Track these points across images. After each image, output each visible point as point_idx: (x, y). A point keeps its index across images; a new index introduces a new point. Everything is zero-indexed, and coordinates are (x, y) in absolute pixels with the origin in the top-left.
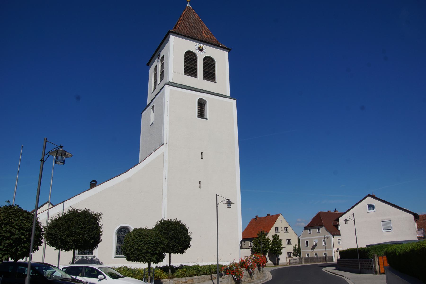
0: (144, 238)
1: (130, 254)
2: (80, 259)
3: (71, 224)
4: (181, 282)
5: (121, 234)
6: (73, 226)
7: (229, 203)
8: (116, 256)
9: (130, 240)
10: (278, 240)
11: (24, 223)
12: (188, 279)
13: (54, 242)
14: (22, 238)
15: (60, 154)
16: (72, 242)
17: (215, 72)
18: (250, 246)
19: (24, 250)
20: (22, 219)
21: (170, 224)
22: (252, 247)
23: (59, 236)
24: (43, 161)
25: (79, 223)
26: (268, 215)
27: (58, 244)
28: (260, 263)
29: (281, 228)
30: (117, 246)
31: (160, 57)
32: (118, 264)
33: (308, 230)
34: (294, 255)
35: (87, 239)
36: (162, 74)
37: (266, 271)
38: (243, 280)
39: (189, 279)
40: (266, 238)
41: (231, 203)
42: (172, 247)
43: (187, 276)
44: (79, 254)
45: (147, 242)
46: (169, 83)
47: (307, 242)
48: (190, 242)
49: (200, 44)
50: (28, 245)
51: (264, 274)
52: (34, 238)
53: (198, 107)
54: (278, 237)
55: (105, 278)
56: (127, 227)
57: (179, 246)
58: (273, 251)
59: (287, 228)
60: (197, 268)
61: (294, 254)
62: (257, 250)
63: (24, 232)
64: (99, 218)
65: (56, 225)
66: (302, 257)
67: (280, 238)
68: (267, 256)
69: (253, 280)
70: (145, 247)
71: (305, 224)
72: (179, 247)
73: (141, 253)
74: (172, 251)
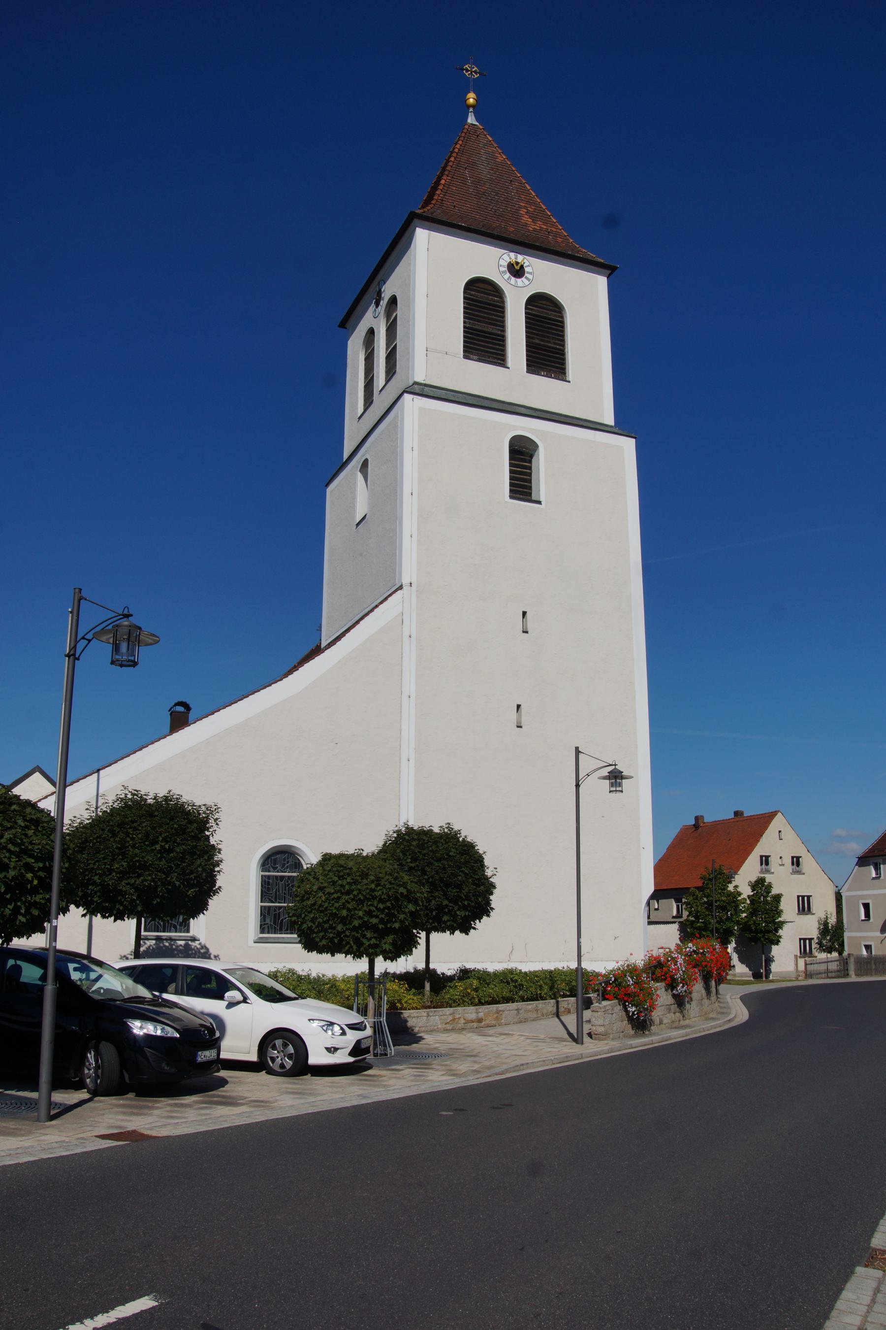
0: (355, 882)
1: (316, 931)
2: (151, 945)
3: (128, 839)
4: (464, 1021)
5: (275, 869)
6: (134, 846)
7: (616, 778)
8: (261, 938)
9: (315, 888)
10: (769, 899)
11: (29, 835)
12: (483, 1010)
13: (80, 894)
14: (28, 880)
15: (125, 637)
16: (135, 892)
17: (563, 346)
18: (675, 913)
19: (35, 912)
20: (22, 824)
21: (429, 841)
22: (681, 917)
23: (96, 875)
24: (73, 656)
25: (151, 837)
26: (737, 813)
27: (95, 899)
28: (710, 967)
29: (781, 858)
30: (261, 907)
31: (382, 302)
33: (869, 865)
34: (822, 948)
35: (177, 883)
36: (391, 357)
37: (728, 997)
38: (657, 1020)
39: (487, 1010)
40: (729, 889)
41: (622, 778)
42: (434, 913)
43: (481, 1003)
44: (149, 931)
45: (365, 896)
46: (416, 386)
47: (866, 906)
48: (491, 897)
49: (512, 255)
50: (44, 898)
51: (722, 1005)
52: (60, 878)
53: (511, 465)
54: (770, 886)
55: (245, 1000)
56: (293, 849)
57: (456, 908)
58: (751, 931)
59: (798, 858)
60: (511, 979)
61: (820, 943)
62: (699, 929)
63: (33, 861)
64: (212, 821)
65: (86, 841)
66: (849, 955)
67: (774, 891)
68: (731, 948)
69: (687, 1022)
70: (360, 910)
71: (860, 848)
72: (458, 913)
73: (346, 928)
74: (436, 924)
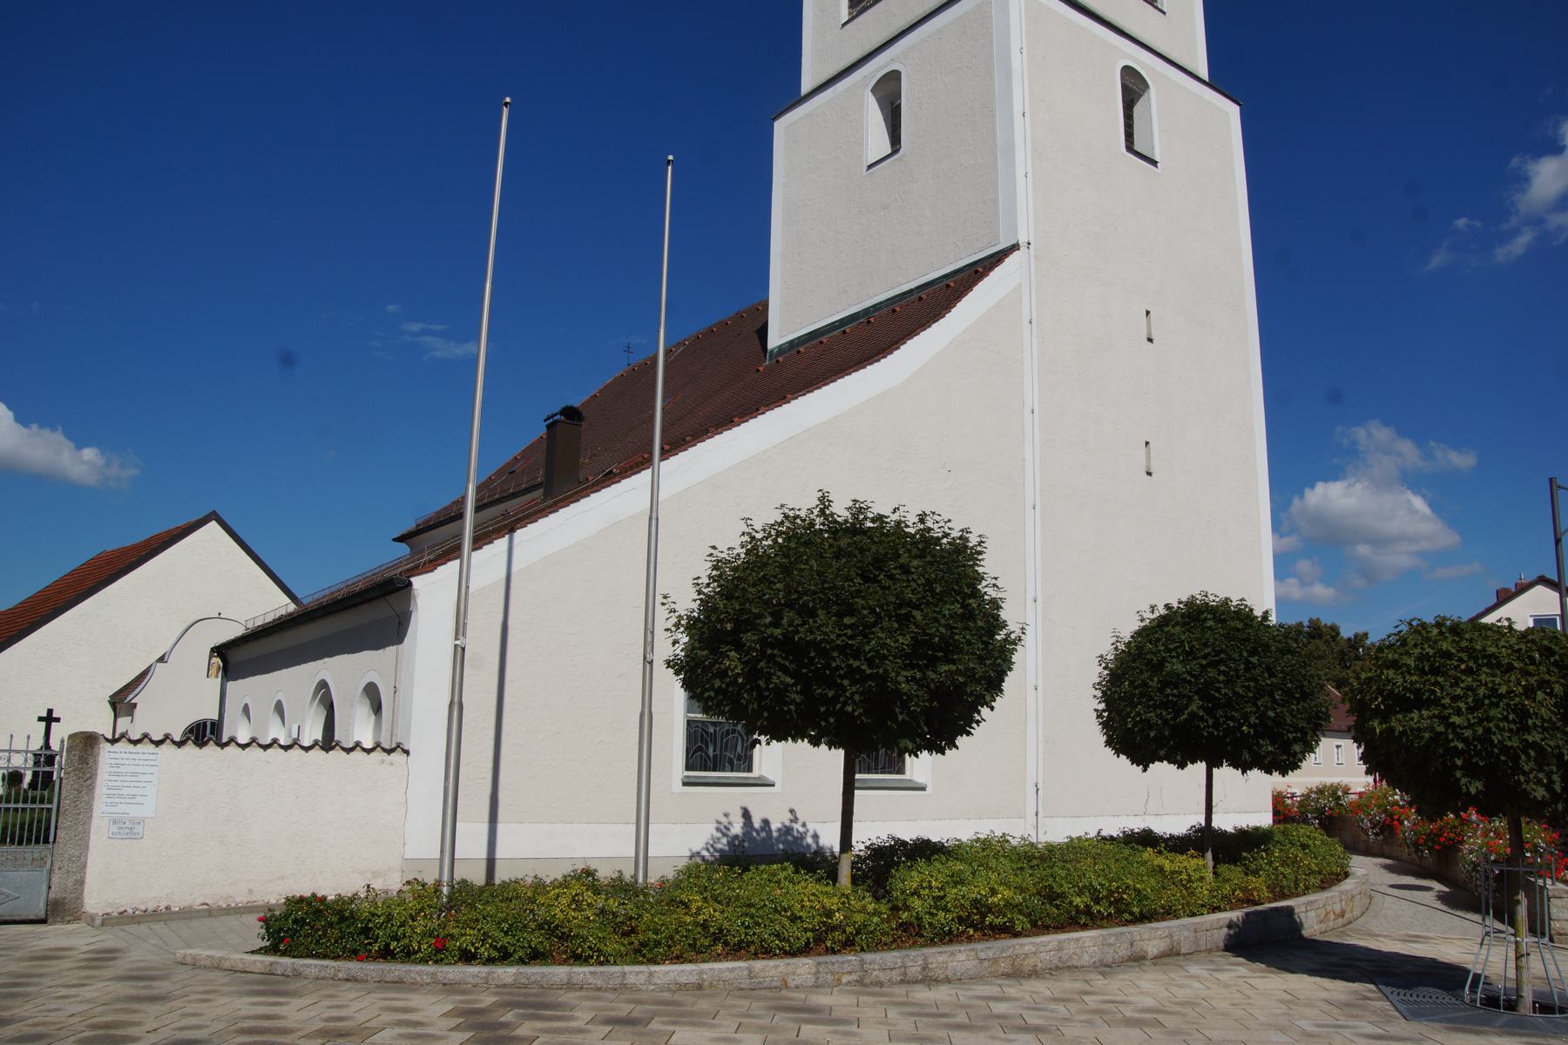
30: (1469, 971)
32: (959, 819)
